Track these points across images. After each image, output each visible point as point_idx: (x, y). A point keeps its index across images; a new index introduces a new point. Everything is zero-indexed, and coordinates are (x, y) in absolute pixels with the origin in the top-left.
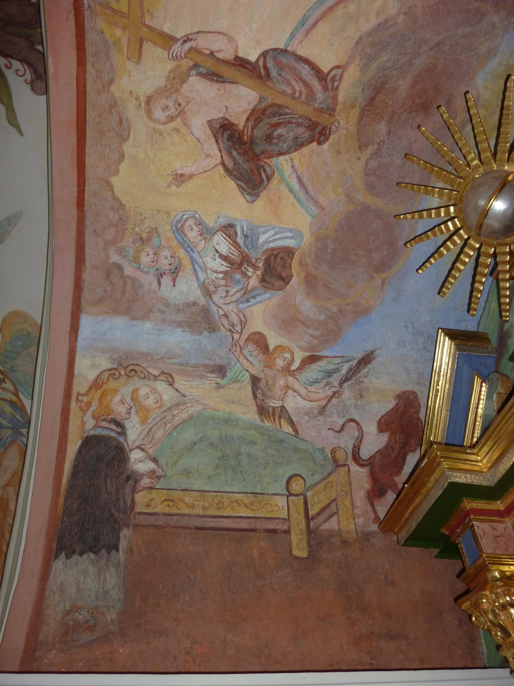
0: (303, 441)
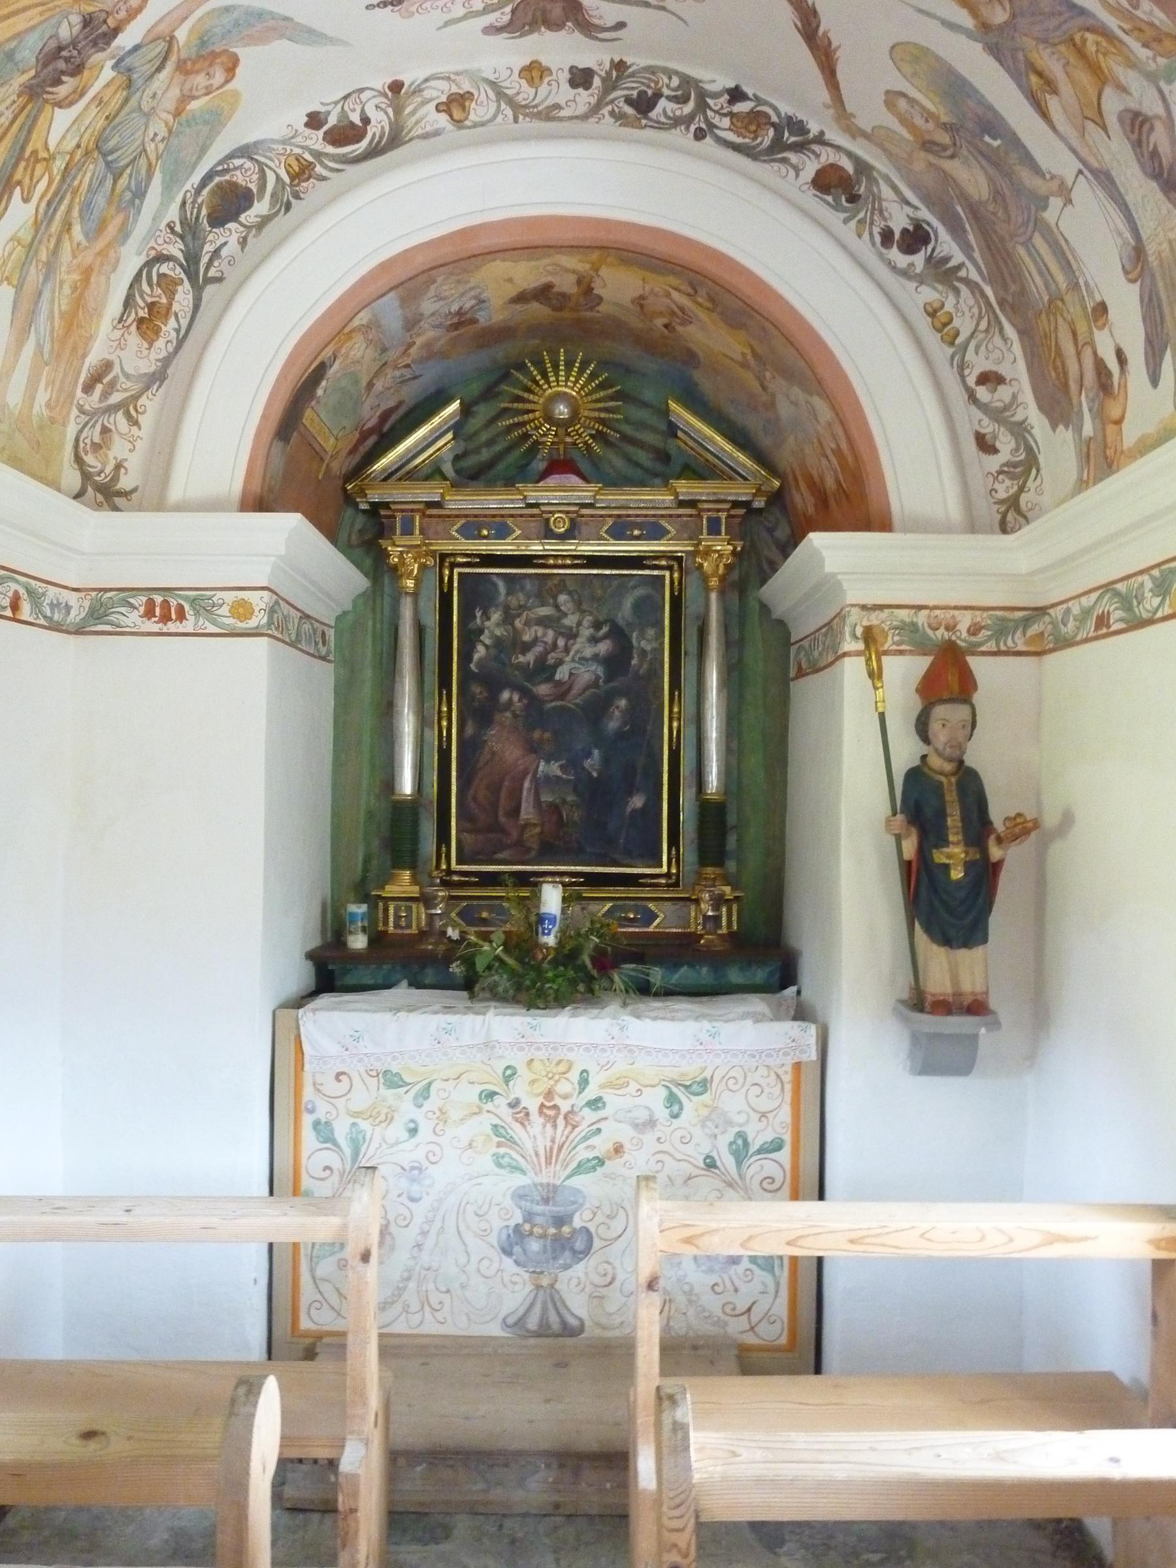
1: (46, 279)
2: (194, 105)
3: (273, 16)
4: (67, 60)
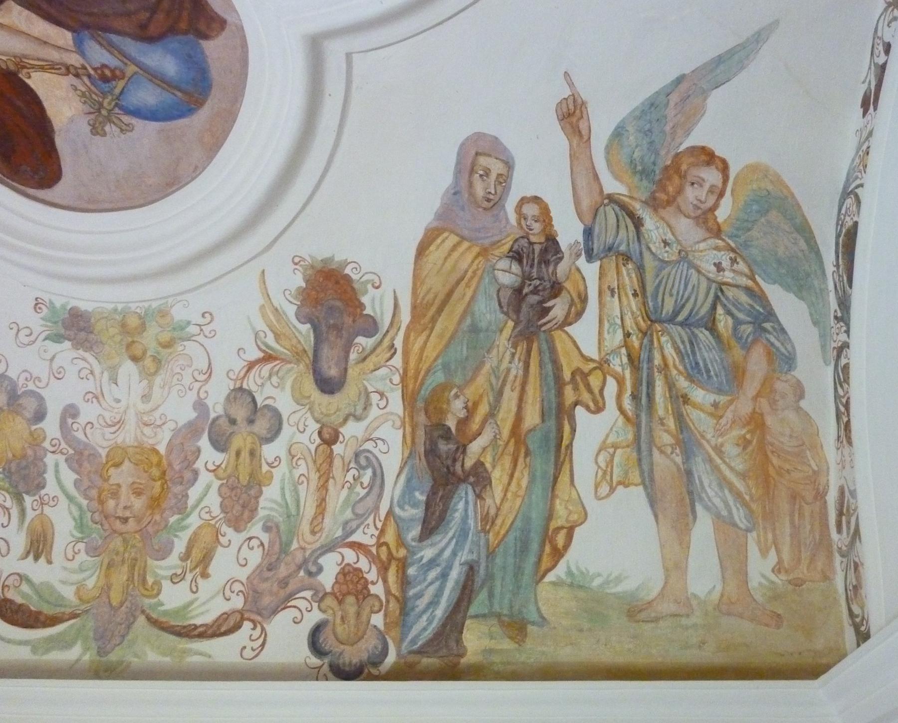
0: (703, 238)
1: (688, 455)
2: (723, 213)
3: (667, 92)
4: (535, 291)
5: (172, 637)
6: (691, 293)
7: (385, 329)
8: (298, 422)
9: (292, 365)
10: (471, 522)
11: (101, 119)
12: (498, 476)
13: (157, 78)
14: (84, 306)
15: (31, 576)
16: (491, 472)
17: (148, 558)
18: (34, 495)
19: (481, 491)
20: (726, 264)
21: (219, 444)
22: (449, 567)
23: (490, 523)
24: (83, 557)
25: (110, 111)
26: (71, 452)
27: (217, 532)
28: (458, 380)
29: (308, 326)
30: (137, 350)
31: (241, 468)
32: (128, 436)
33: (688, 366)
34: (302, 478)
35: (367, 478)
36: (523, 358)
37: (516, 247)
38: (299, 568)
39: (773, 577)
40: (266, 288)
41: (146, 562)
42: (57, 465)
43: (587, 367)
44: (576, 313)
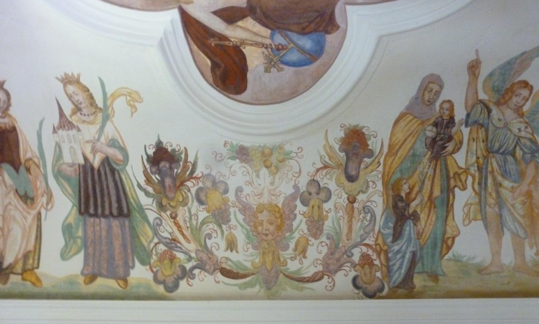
1: (501, 207)
2: (525, 108)
4: (441, 140)
5: (297, 283)
6: (506, 141)
7: (376, 155)
8: (338, 194)
9: (336, 170)
10: (412, 235)
11: (270, 66)
12: (423, 216)
13: (301, 50)
14: (246, 144)
15: (231, 258)
16: (420, 215)
17: (279, 251)
18: (226, 225)
19: (416, 223)
20: (523, 129)
21: (305, 203)
22: (405, 253)
23: (420, 235)
24: (251, 250)
25: (275, 63)
26: (241, 206)
27: (307, 240)
28: (406, 176)
29: (344, 153)
30: (268, 164)
31: (314, 213)
32: (265, 200)
33: (502, 171)
34: (341, 217)
35: (368, 217)
36: (434, 167)
37: (436, 121)
38: (344, 254)
39: (535, 257)
40: (327, 137)
41: (278, 252)
42: (235, 212)
43: (460, 171)
44: (457, 149)
